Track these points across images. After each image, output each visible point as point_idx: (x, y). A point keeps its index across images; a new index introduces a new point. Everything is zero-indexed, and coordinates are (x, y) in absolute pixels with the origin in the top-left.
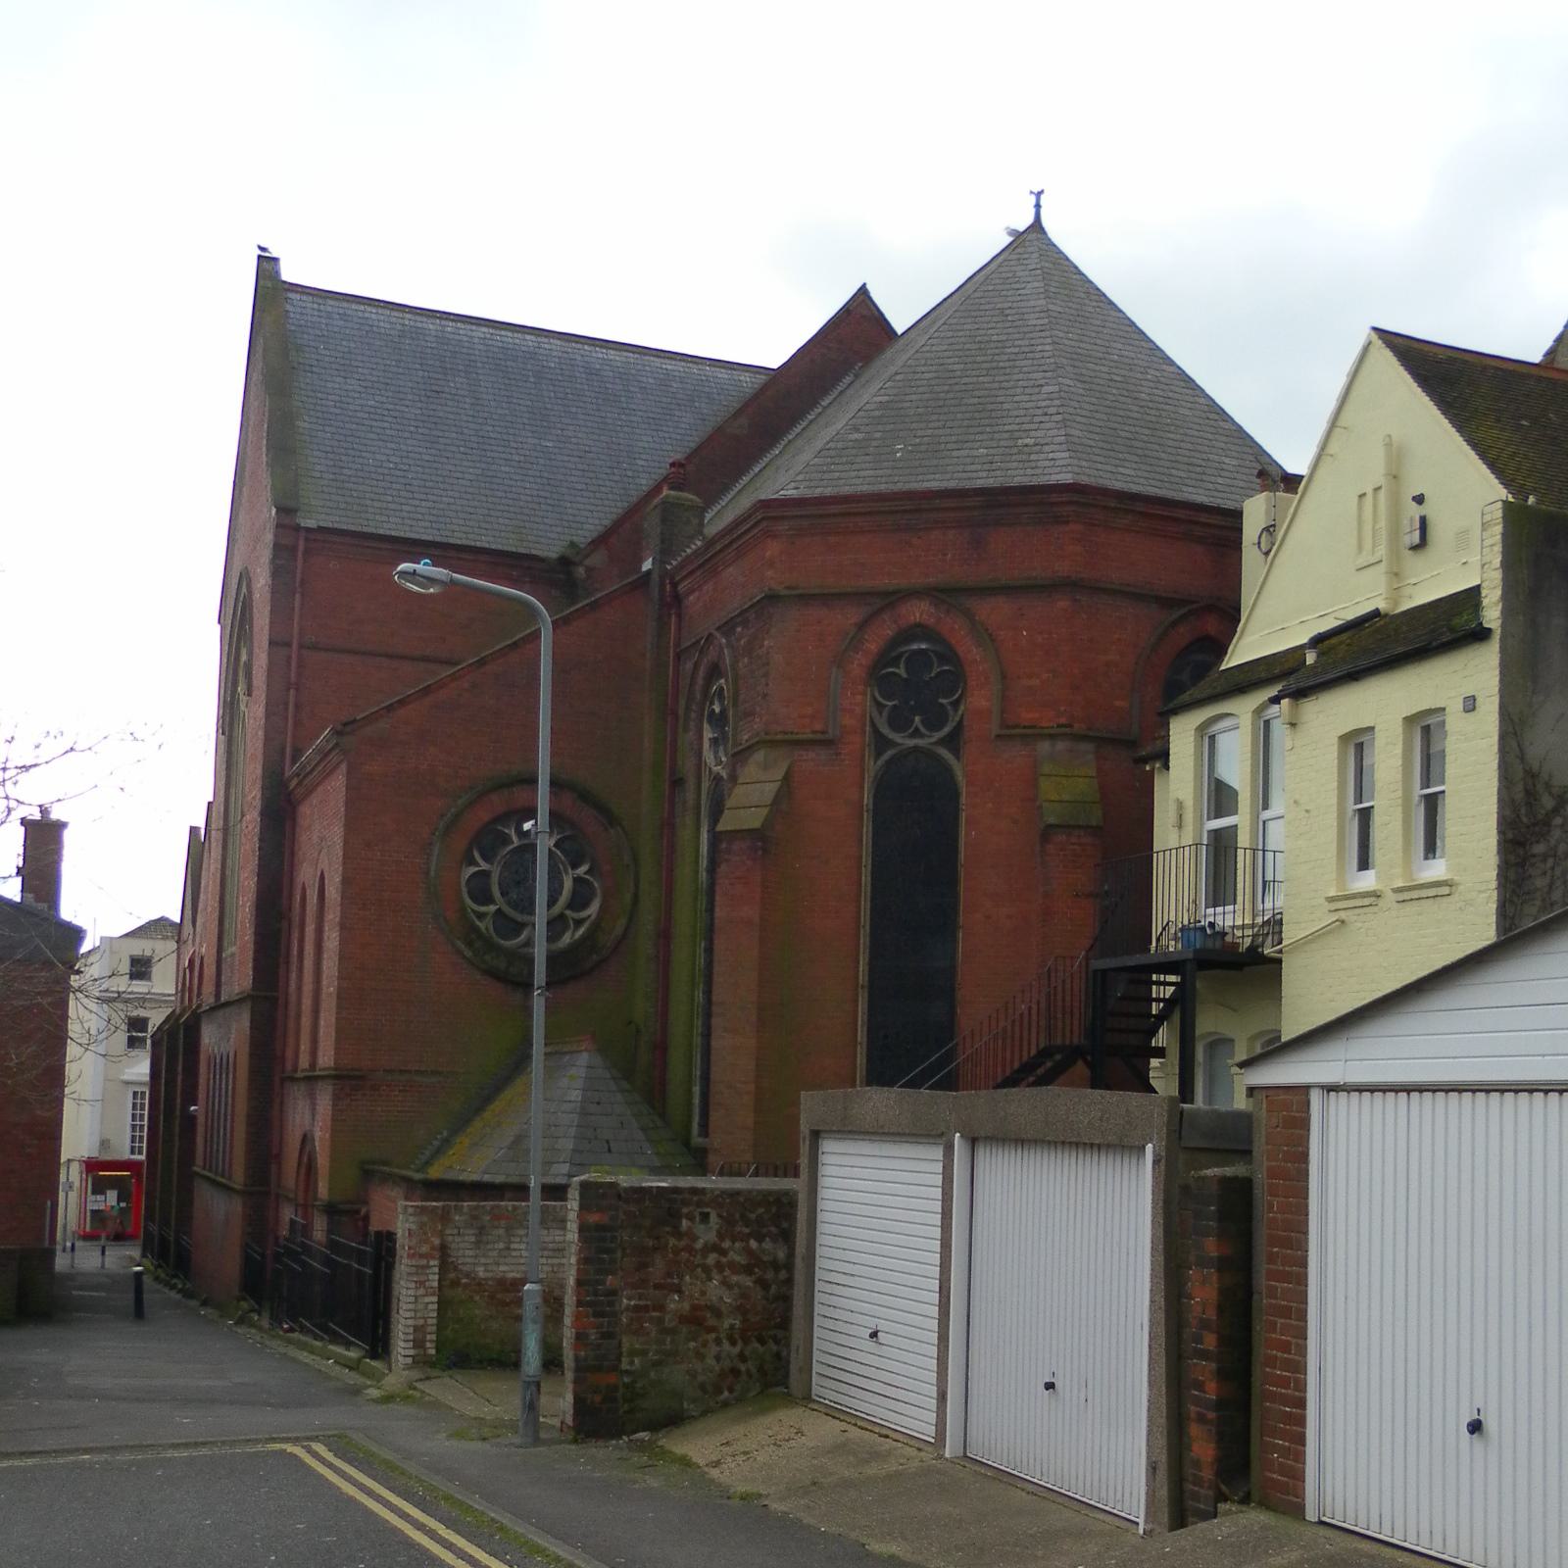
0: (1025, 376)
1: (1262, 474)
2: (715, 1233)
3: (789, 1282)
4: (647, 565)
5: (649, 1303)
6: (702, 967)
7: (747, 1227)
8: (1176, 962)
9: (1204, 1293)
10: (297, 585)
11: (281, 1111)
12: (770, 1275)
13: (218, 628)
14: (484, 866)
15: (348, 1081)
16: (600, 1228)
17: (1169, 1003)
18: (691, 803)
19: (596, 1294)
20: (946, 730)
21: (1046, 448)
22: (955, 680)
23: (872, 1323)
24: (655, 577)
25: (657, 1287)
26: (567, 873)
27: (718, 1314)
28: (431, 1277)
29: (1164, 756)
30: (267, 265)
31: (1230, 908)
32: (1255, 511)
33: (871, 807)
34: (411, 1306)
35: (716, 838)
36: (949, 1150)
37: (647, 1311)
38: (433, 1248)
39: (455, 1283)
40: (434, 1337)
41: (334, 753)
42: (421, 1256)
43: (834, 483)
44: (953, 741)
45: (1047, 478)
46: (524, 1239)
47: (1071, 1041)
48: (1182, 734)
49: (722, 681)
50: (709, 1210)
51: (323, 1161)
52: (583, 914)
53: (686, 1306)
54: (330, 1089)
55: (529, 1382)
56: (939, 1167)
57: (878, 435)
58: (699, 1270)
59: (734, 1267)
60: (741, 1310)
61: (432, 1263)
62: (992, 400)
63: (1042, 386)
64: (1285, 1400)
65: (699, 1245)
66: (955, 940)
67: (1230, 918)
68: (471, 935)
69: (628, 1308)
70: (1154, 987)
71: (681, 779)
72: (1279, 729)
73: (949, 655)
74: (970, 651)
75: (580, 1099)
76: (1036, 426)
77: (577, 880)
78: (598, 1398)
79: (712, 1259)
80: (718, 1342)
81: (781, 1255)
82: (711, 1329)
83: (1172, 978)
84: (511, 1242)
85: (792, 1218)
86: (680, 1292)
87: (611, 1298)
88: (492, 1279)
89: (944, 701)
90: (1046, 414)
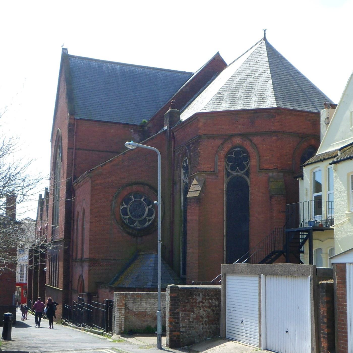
0: (263, 79)
1: (325, 104)
2: (201, 299)
3: (220, 310)
4: (165, 128)
5: (186, 315)
6: (182, 231)
7: (209, 297)
8: (308, 230)
9: (323, 310)
10: (75, 133)
11: (72, 269)
12: (214, 308)
13: (50, 143)
14: (126, 206)
15: (93, 262)
16: (175, 297)
17: (305, 240)
18: (178, 189)
19: (174, 313)
20: (245, 170)
21: (269, 98)
22: (247, 158)
23: (241, 319)
24: (168, 131)
25: (189, 311)
26: (146, 207)
27: (202, 317)
28: (123, 311)
29: (302, 176)
30: (64, 51)
31: (320, 215)
32: (324, 113)
33: (226, 190)
34: (118, 318)
35: (186, 199)
36: (260, 278)
37: (186, 317)
38: (123, 304)
39: (128, 313)
40: (124, 326)
41: (87, 178)
42: (120, 306)
43: (215, 108)
44: (247, 173)
45: (270, 106)
46: (145, 301)
47: (278, 249)
48: (307, 171)
49: (187, 158)
50: (200, 293)
51: (86, 283)
52: (151, 218)
53: (195, 316)
54: (88, 264)
55: (159, 334)
56: (258, 282)
57: (226, 95)
58: (198, 307)
59: (206, 307)
60: (208, 317)
61: (123, 308)
62: (255, 85)
63: (267, 81)
64: (343, 332)
65: (198, 301)
66: (248, 224)
67: (320, 219)
68: (123, 224)
69: (182, 316)
70: (301, 236)
71: (176, 183)
72: (331, 171)
73: (245, 151)
74: (251, 150)
75: (153, 266)
76: (266, 92)
77: (149, 209)
78: (175, 338)
79: (201, 304)
80: (203, 324)
81: (217, 303)
82: (201, 321)
83: (306, 233)
84: (141, 302)
85: (219, 295)
86: (194, 312)
87: (178, 314)
88: (137, 312)
89: (244, 163)
90: (269, 89)
